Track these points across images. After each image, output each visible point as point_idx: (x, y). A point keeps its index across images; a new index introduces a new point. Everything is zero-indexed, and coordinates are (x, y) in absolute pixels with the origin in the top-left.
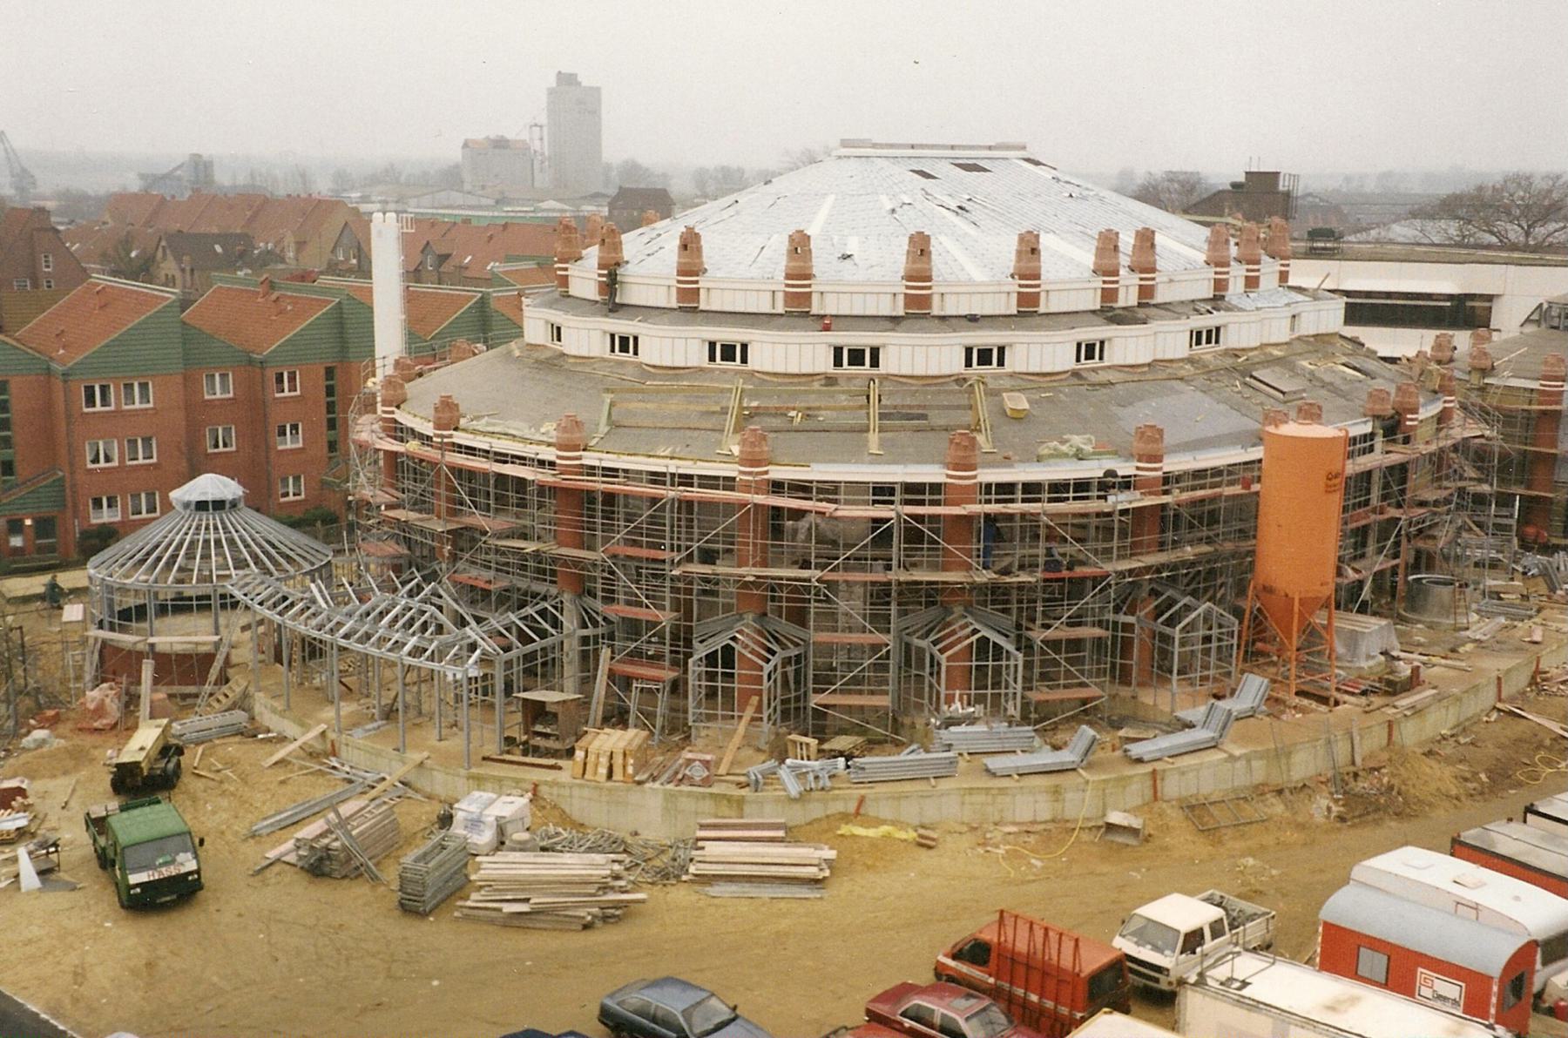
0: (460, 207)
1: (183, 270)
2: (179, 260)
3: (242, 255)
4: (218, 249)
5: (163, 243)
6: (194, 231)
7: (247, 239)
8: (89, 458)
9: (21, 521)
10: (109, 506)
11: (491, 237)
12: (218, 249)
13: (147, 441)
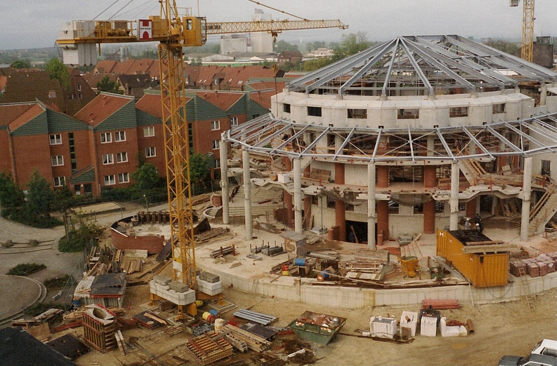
0: (221, 61)
1: (126, 88)
2: (124, 85)
3: (148, 82)
4: (138, 80)
5: (118, 79)
6: (128, 74)
7: (148, 76)
8: (103, 162)
9: (79, 185)
10: (111, 179)
11: (239, 72)
12: (138, 80)
13: (124, 154)
